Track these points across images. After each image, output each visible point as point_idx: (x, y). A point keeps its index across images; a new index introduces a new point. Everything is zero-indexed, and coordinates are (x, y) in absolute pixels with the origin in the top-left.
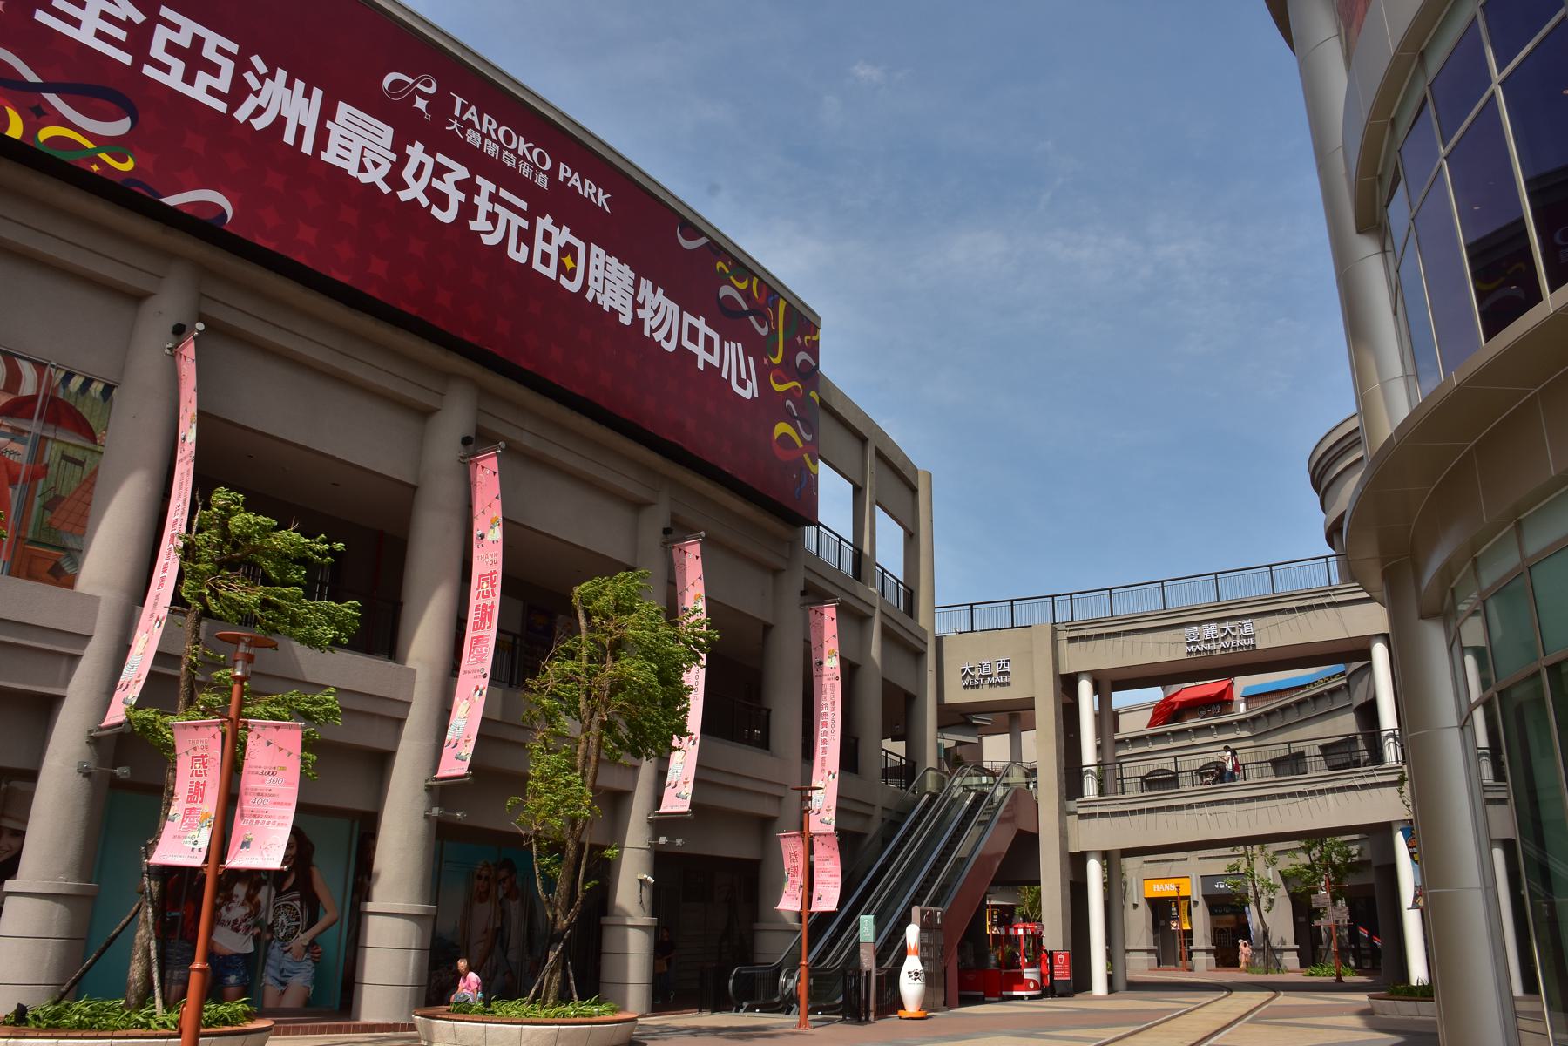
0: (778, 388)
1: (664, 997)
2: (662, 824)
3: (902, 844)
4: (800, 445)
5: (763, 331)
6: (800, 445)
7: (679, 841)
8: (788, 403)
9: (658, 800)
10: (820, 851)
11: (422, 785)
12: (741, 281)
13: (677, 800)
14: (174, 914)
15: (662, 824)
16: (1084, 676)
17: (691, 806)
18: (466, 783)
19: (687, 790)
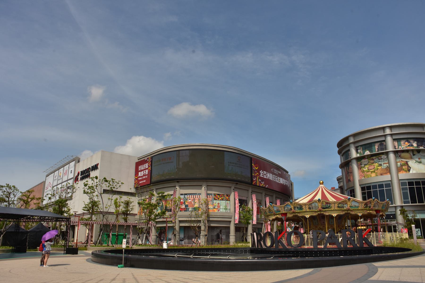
0: (258, 173)
1: (365, 187)
2: (253, 225)
3: (370, 156)
4: (255, 167)
5: (260, 180)
6: (255, 167)
7: (237, 226)
8: (256, 172)
9: (253, 223)
10: (268, 226)
11: (234, 224)
12: (262, 185)
13: (255, 222)
14: (382, 221)
15: (235, 224)
16: (388, 136)
17: (257, 223)
18: (343, 235)
19: (256, 221)
